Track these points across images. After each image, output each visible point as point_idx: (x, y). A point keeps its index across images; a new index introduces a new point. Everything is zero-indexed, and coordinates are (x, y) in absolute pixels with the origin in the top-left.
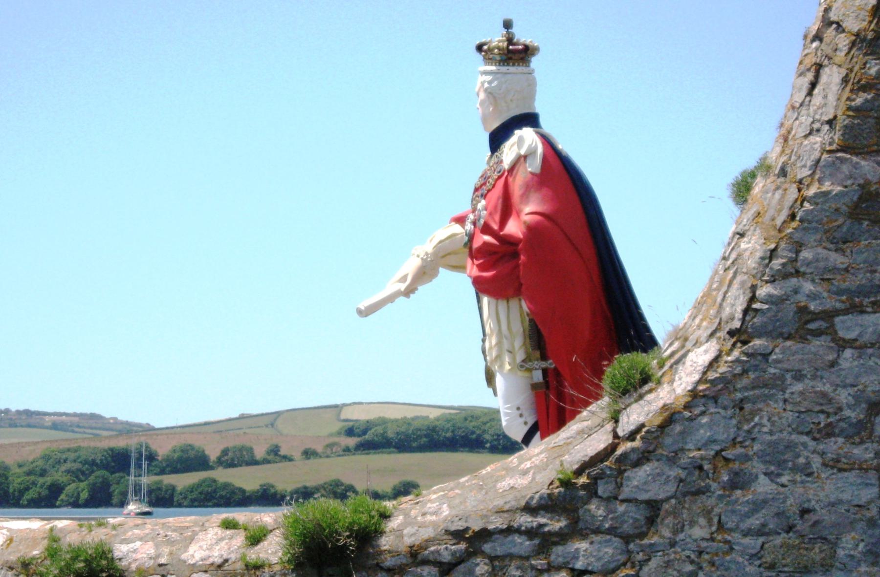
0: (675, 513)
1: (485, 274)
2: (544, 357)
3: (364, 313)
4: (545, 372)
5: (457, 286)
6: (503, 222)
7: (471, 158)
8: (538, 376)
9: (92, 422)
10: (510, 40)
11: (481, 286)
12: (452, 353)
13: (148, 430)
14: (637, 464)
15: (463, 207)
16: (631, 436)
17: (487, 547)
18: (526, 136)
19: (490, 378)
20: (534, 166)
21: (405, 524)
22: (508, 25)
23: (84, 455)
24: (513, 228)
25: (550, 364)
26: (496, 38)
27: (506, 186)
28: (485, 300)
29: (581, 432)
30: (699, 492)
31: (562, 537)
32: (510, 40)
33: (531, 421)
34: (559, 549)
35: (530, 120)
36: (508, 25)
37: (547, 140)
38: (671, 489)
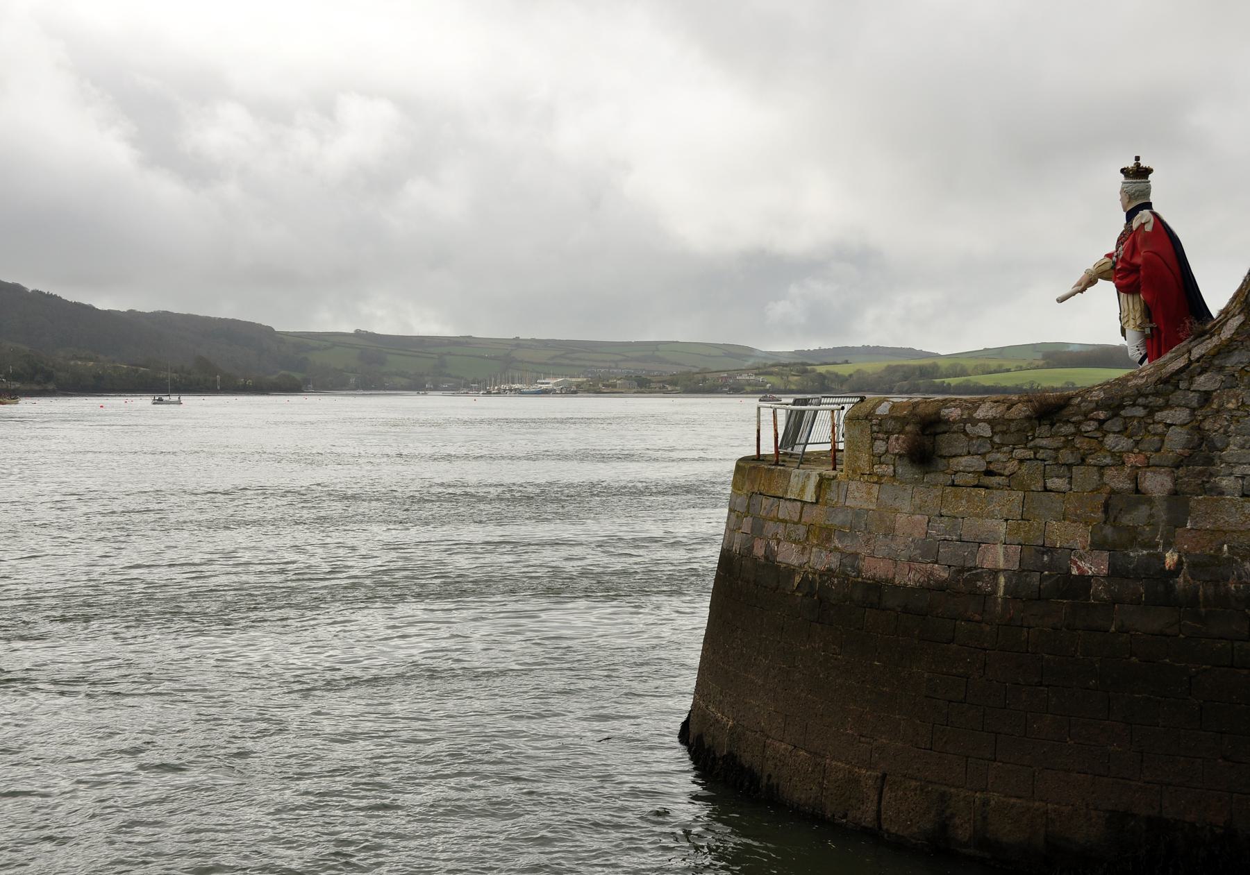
0: (1219, 397)
1: (1124, 282)
2: (1151, 322)
3: (1061, 300)
4: (1152, 329)
5: (1106, 290)
6: (1131, 257)
7: (1117, 223)
8: (1148, 331)
9: (910, 352)
10: (1138, 165)
11: (1120, 289)
12: (1102, 320)
13: (938, 356)
14: (1200, 374)
15: (1112, 249)
16: (1198, 360)
17: (1122, 413)
18: (1145, 215)
19: (1123, 333)
20: (1149, 228)
21: (1081, 402)
22: (1137, 158)
23: (700, 535)
24: (1138, 260)
25: (1154, 325)
26: (1130, 164)
27: (1134, 239)
28: (733, 429)
29: (1171, 358)
30: (1233, 387)
31: (1161, 409)
32: (1138, 165)
33: (1143, 352)
34: (1159, 414)
35: (1148, 205)
36: (1137, 158)
37: (1156, 215)
38: (1217, 385)
